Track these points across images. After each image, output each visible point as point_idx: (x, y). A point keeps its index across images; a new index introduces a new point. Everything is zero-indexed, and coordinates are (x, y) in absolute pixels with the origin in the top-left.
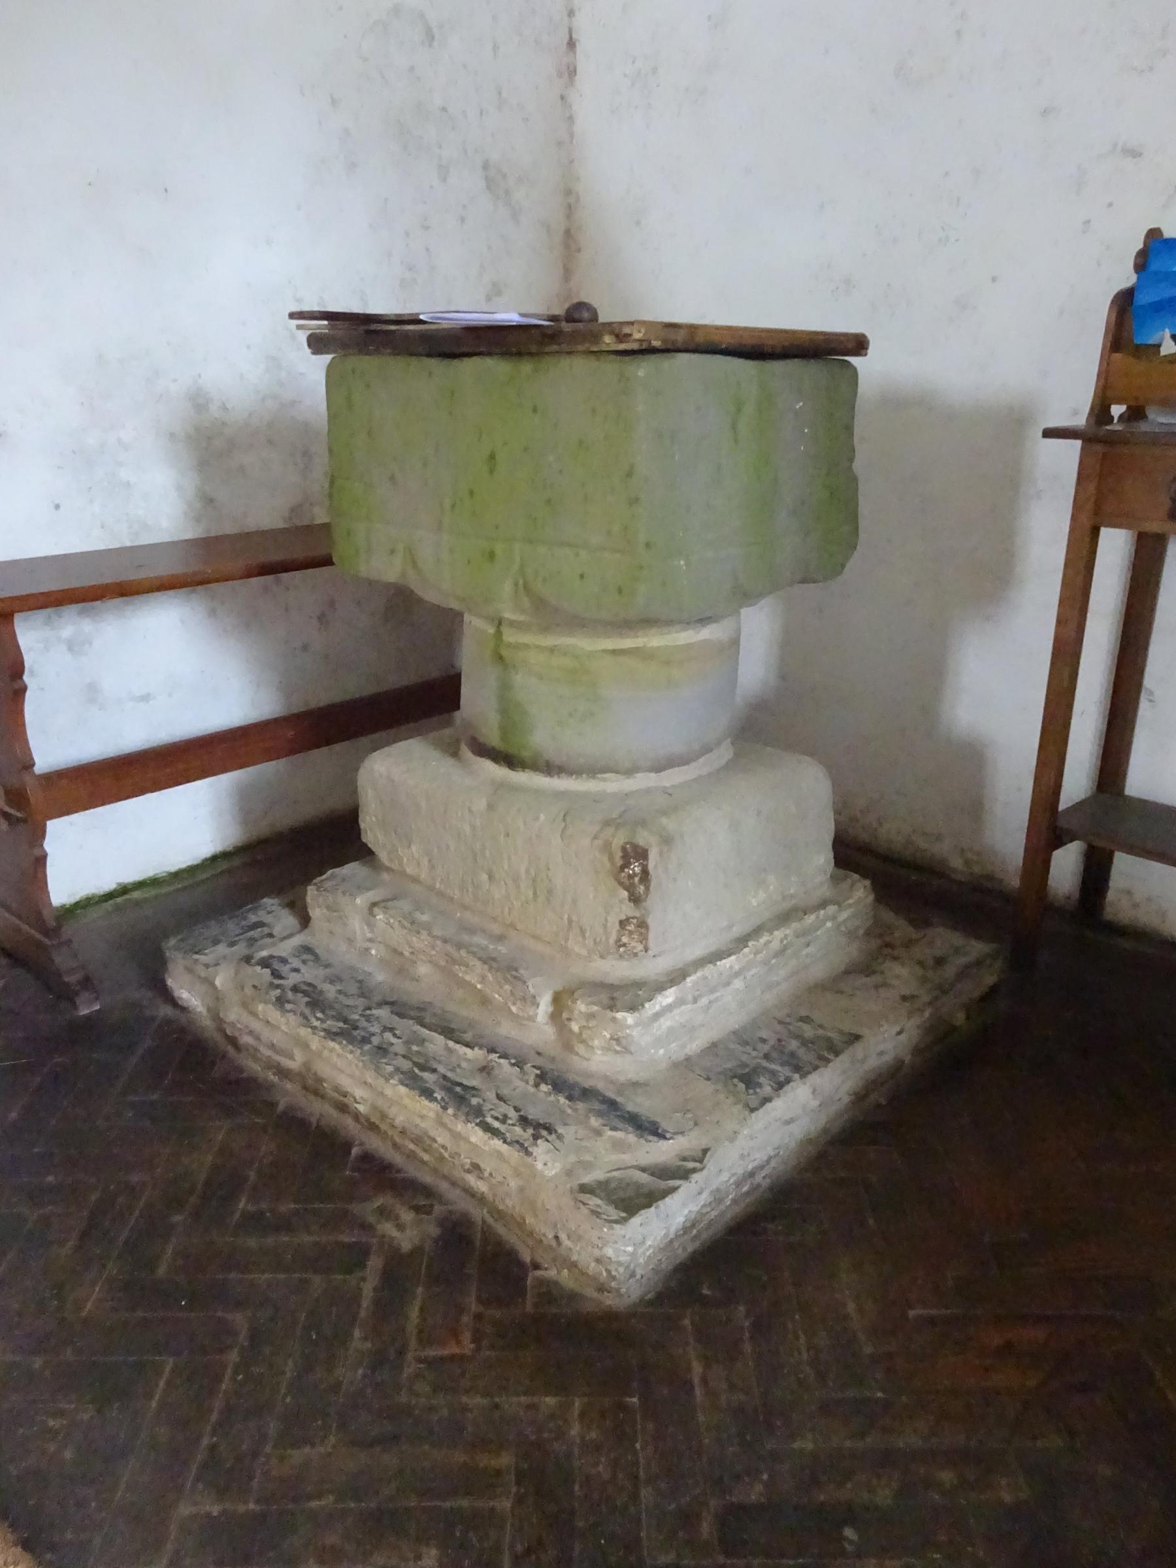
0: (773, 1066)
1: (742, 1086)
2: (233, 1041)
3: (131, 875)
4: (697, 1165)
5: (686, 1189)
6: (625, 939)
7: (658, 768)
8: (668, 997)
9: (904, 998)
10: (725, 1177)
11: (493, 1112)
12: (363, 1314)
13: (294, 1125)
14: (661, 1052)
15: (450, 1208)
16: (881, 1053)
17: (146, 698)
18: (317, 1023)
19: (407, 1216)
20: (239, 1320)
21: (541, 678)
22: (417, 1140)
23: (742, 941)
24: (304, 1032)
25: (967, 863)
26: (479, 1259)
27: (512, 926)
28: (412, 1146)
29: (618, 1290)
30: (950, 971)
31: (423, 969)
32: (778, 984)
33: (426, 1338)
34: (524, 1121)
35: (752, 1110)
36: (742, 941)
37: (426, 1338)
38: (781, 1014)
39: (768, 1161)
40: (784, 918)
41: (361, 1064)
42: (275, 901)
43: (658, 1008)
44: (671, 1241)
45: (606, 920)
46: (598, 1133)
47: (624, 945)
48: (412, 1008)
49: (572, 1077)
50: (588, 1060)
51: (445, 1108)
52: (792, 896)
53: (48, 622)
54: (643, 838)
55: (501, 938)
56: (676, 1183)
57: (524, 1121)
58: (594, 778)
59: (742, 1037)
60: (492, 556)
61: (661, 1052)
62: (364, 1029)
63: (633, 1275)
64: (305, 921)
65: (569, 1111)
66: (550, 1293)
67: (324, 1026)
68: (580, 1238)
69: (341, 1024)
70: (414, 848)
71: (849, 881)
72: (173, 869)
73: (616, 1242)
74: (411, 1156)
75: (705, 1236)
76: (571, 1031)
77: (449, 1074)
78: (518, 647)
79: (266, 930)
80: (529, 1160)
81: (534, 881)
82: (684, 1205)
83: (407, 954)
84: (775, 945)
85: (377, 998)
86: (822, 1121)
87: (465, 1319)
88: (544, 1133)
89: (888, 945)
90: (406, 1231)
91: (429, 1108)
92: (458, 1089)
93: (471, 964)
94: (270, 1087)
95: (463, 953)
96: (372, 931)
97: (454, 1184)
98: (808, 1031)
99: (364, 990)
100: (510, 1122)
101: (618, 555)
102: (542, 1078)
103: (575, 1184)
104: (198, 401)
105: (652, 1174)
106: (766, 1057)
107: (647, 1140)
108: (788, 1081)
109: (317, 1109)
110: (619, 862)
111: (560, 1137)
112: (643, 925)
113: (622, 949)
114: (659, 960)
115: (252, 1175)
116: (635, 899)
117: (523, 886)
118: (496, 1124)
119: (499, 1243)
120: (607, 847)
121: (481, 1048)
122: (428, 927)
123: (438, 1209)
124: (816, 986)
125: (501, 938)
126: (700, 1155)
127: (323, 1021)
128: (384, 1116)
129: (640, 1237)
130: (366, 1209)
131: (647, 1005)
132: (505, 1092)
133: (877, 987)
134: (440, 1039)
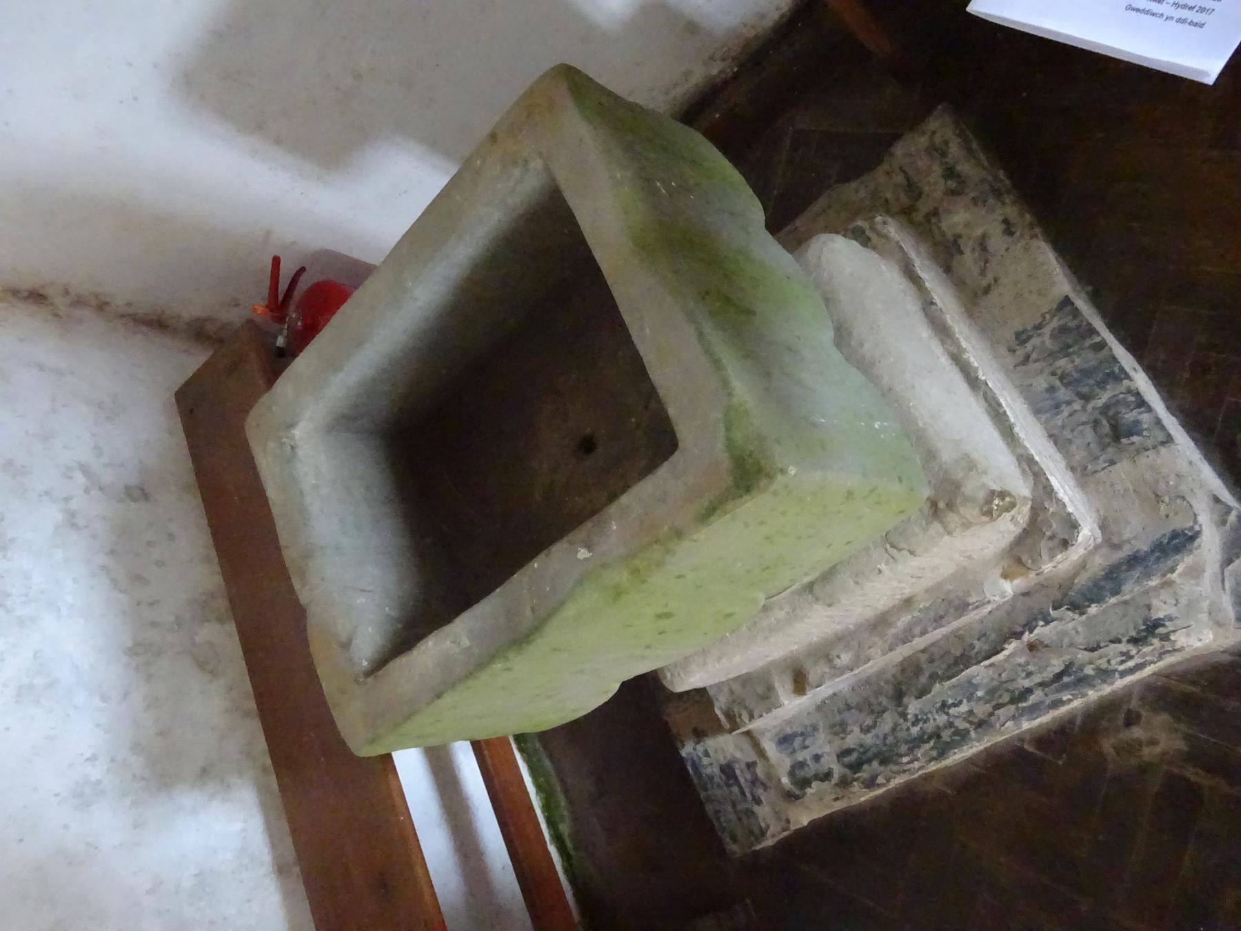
11: (1113, 662)
118: (1131, 664)
126: (1219, 506)
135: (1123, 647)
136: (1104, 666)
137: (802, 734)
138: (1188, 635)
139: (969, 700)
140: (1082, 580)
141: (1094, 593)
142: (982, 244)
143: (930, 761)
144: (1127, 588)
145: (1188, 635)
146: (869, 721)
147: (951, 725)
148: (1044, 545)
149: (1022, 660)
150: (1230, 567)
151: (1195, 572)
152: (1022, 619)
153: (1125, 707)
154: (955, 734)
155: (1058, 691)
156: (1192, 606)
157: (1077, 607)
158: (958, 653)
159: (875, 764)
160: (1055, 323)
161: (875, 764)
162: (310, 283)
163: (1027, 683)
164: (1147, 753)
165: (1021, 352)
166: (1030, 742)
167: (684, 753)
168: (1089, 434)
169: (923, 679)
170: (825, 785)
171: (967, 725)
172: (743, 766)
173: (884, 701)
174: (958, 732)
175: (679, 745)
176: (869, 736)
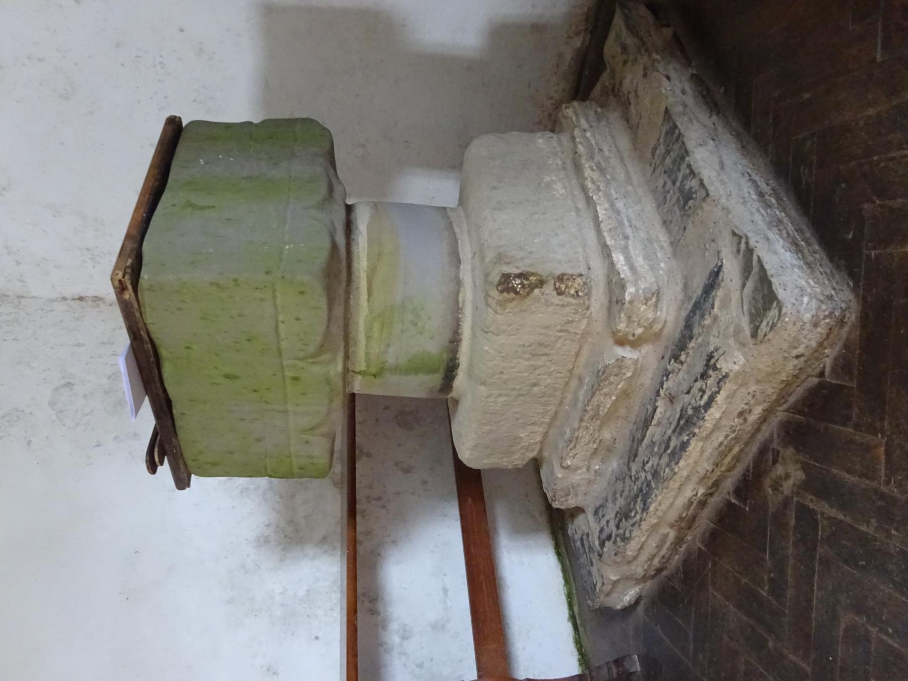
0: (680, 178)
1: (691, 203)
2: (659, 571)
3: (563, 611)
4: (743, 240)
5: (762, 251)
6: (572, 291)
7: (457, 261)
8: (619, 259)
9: (645, 75)
10: (758, 218)
12: (848, 520)
13: (714, 539)
14: (662, 265)
15: (775, 435)
16: (683, 92)
17: (445, 591)
18: (638, 517)
19: (779, 470)
20: (846, 619)
21: (388, 346)
22: (723, 455)
23: (589, 201)
24: (645, 526)
25: (577, 34)
26: (813, 417)
27: (571, 371)
28: (729, 459)
29: (843, 311)
30: (630, 41)
31: (607, 435)
32: (627, 173)
33: (869, 473)
34: (704, 376)
35: (708, 195)
36: (589, 201)
37: (869, 473)
38: (649, 170)
39: (754, 182)
40: (578, 168)
41: (665, 490)
42: (570, 526)
43: (625, 268)
44: (807, 264)
45: (558, 305)
46: (715, 319)
47: (577, 292)
48: (632, 447)
49: (677, 335)
50: (665, 322)
51: (694, 435)
52: (564, 163)
53: (389, 651)
54: (495, 277)
55: (580, 379)
56: (755, 258)
57: (704, 376)
58: (462, 309)
59: (661, 201)
61: (662, 265)
62: (642, 483)
63: (830, 297)
64: (579, 510)
65: (700, 340)
66: (843, 365)
67: (640, 511)
68: (796, 339)
69: (639, 499)
70: (522, 435)
71: (562, 119)
72: (563, 582)
73: (798, 311)
74: (737, 459)
75: (808, 235)
76: (643, 333)
77: (672, 428)
78: (368, 360)
79: (585, 537)
80: (731, 375)
81: (533, 355)
82: (775, 253)
83: (595, 446)
84: (595, 175)
85: (626, 468)
86: (727, 137)
88: (713, 361)
89: (613, 90)
90: (789, 473)
91: (695, 447)
92: (682, 422)
93: (596, 403)
94: (689, 552)
95: (589, 408)
96: (580, 468)
97: (758, 430)
98: (661, 149)
99: (620, 478)
100: (704, 387)
101: (278, 294)
102: (676, 357)
103: (751, 341)
104: (263, 542)
105: (747, 278)
106: (674, 183)
107: (723, 280)
108: (689, 166)
109: (705, 521)
110: (512, 295)
111: (717, 349)
112: (561, 278)
113: (580, 294)
114: (591, 263)
115: (744, 580)
116: (541, 283)
117: (540, 363)
118: (706, 398)
120: (502, 304)
121: (656, 401)
122: (574, 431)
123: (775, 445)
124: (634, 144)
125: (580, 379)
127: (636, 513)
128: (705, 477)
129: (796, 291)
130: (773, 500)
131: (622, 276)
132: (685, 387)
133: (637, 96)
134: (651, 429)
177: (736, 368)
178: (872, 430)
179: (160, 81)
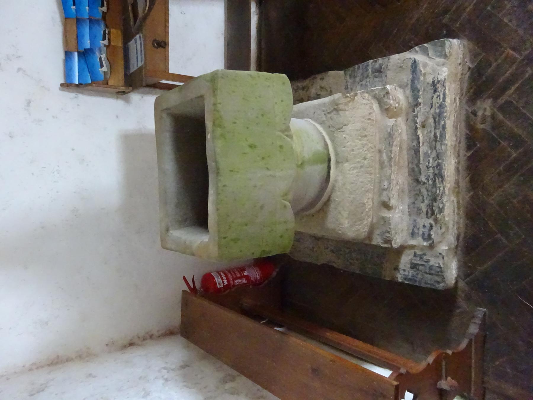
11: (438, 102)
18: (442, 189)
33: (513, 61)
60: (281, 147)
87: (499, 61)
113: (315, 250)
118: (442, 96)
119: (470, 84)
135: (435, 96)
136: (438, 105)
137: (414, 227)
138: (441, 75)
139: (430, 157)
140: (411, 99)
141: (416, 98)
142: (322, 88)
143: (443, 183)
144: (419, 86)
145: (441, 75)
146: (421, 198)
147: (434, 168)
148: (385, 100)
149: (426, 132)
150: (430, 55)
151: (425, 65)
152: (413, 125)
153: (470, 113)
154: (437, 168)
155: (439, 124)
156: (434, 71)
157: (417, 105)
158: (413, 152)
159: (435, 204)
160: (348, 77)
161: (435, 204)
162: (200, 280)
163: (433, 134)
164: (488, 113)
165: (349, 90)
166: (467, 151)
167: (400, 280)
168: (377, 80)
169: (416, 169)
170: (434, 228)
171: (436, 162)
172: (414, 258)
173: (417, 188)
174: (437, 166)
175: (396, 280)
176: (425, 201)
177: (446, 73)
178: (504, 52)
179: (55, 182)
